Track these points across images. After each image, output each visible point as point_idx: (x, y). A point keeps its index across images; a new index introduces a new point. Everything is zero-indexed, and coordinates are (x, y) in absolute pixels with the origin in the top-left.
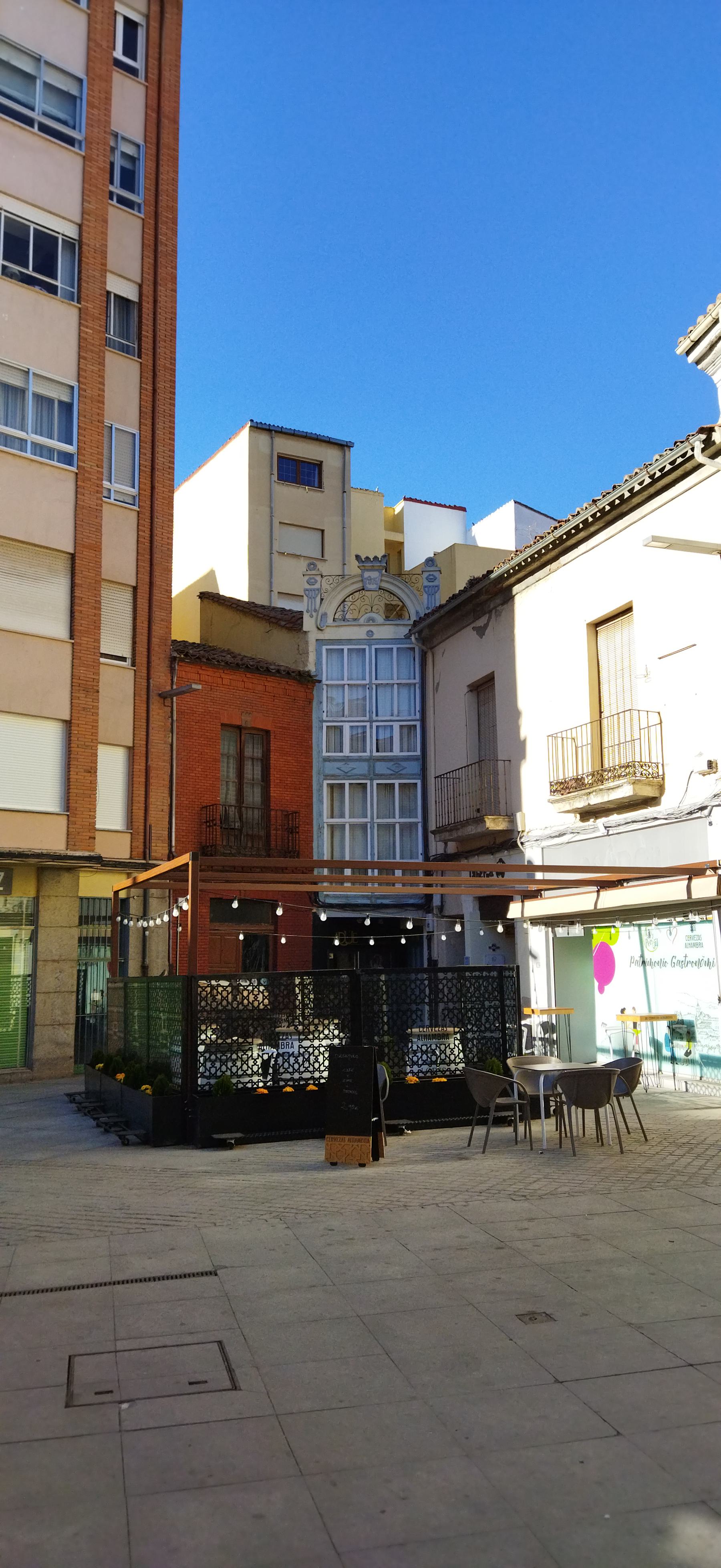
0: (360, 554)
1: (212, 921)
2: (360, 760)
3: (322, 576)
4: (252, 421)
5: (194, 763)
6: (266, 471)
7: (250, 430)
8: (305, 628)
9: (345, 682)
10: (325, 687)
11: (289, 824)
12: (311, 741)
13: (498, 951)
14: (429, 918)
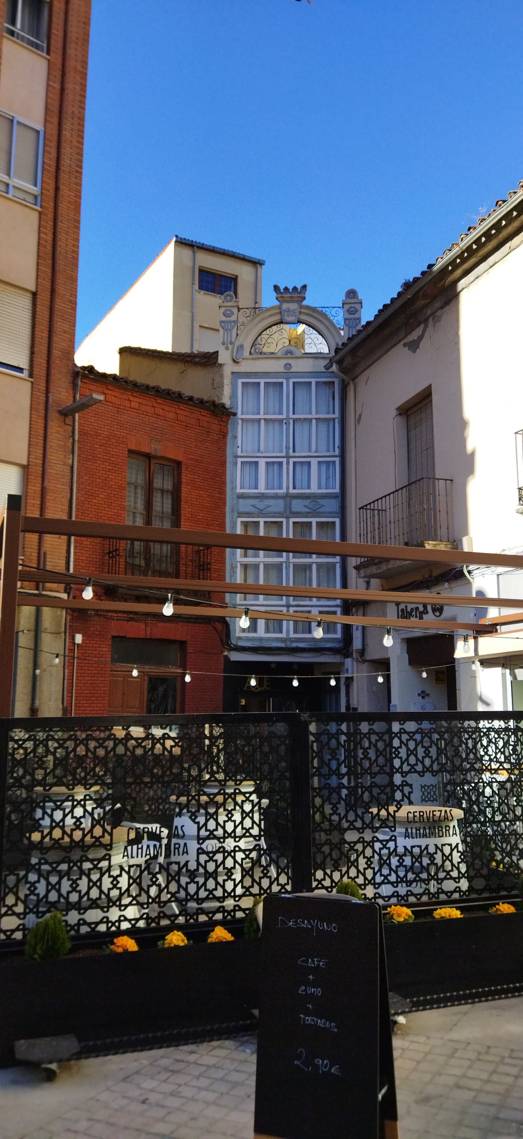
0: (279, 285)
1: (113, 661)
2: (276, 497)
3: (239, 309)
4: (177, 236)
5: (97, 489)
6: (189, 281)
7: (175, 245)
8: (220, 361)
9: (262, 416)
10: (240, 422)
11: (200, 560)
12: (225, 476)
13: (427, 698)
14: (348, 662)
